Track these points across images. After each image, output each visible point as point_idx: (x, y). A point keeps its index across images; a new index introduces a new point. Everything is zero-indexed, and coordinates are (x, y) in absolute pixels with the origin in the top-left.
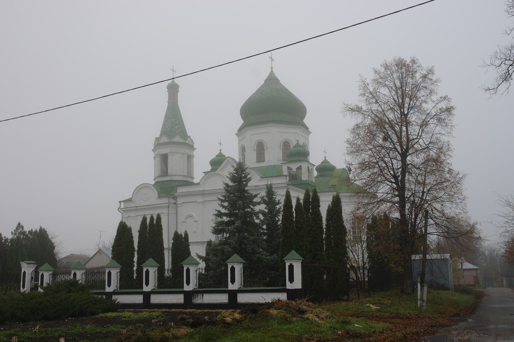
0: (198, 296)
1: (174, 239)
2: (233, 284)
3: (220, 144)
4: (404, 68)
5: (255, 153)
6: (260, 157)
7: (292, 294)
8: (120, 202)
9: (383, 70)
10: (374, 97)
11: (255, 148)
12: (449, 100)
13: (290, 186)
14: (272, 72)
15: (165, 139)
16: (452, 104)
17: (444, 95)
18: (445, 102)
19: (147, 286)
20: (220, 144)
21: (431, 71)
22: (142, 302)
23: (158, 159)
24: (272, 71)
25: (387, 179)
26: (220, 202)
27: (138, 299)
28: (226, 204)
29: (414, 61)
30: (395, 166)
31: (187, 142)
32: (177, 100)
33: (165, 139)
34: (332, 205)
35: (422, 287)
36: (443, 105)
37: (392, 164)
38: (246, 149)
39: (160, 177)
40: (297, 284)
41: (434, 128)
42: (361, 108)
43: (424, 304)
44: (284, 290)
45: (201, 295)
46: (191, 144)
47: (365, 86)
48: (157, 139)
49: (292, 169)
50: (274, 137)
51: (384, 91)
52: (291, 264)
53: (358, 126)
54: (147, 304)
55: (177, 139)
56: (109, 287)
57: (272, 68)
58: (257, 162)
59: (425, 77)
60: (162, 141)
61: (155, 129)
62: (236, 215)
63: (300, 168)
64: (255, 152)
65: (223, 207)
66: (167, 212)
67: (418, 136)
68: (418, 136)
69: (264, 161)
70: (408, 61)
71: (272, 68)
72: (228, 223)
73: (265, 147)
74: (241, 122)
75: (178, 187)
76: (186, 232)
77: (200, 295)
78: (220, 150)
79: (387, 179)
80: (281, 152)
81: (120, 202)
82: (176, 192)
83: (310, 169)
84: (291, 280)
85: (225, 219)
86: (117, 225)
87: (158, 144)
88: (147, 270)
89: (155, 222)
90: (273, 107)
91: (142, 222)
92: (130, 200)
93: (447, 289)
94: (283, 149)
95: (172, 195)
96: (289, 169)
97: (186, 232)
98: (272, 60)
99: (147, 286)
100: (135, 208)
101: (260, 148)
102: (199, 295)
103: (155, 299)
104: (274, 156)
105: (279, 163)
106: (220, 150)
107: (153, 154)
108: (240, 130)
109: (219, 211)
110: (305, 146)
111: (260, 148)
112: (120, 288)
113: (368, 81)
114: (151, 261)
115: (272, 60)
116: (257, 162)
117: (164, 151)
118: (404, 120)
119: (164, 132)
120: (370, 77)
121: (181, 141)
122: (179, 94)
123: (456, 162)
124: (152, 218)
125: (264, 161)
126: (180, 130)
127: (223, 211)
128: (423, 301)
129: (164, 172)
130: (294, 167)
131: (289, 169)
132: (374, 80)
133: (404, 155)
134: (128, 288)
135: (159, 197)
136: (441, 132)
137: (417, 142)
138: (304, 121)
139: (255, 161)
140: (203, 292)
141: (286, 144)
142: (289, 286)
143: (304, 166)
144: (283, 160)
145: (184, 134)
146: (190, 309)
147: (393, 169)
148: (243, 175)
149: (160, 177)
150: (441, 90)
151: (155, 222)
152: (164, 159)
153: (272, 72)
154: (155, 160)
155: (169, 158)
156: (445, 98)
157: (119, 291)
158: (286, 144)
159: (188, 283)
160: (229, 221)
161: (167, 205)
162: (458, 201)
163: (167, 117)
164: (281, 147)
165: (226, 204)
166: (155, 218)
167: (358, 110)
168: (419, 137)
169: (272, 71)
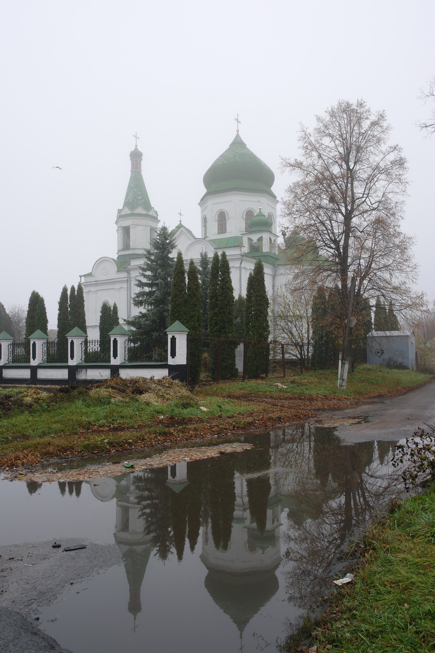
0: (82, 371)
1: (102, 312)
2: (115, 358)
3: (180, 214)
4: (350, 113)
5: (216, 224)
6: (222, 229)
7: (172, 369)
8: (81, 277)
9: (328, 118)
10: (311, 147)
11: (217, 219)
12: (400, 150)
13: (244, 257)
14: (238, 135)
15: (127, 211)
16: (403, 155)
17: (393, 144)
18: (396, 152)
19: (34, 360)
20: (180, 214)
21: (382, 117)
22: (29, 377)
23: (121, 231)
24: (238, 134)
25: (326, 245)
26: (141, 271)
27: (26, 374)
28: (149, 273)
29: (361, 105)
30: (336, 231)
31: (150, 213)
32: (140, 169)
33: (127, 211)
34: (254, 273)
35: (343, 364)
36: (392, 157)
37: (332, 226)
38: (208, 219)
39: (122, 250)
40: (181, 358)
41: (386, 186)
42: (302, 163)
43: (344, 384)
44: (166, 366)
45: (85, 370)
46: (154, 215)
47: (306, 137)
48: (120, 211)
49: (252, 240)
50: (237, 206)
51: (326, 141)
52: (173, 337)
53: (297, 185)
54: (34, 379)
55: (140, 210)
56: (72, 359)
57: (238, 131)
58: (218, 233)
59: (374, 124)
60: (123, 213)
61: (118, 199)
62: (157, 285)
63: (260, 239)
64: (217, 222)
65: (145, 276)
66: (126, 286)
67: (364, 194)
68: (364, 194)
69: (225, 232)
70: (354, 102)
71: (238, 131)
72: (150, 294)
73: (227, 218)
74: (204, 191)
75: (131, 260)
76: (115, 304)
77: (84, 370)
78: (180, 221)
79: (326, 245)
80: (244, 222)
81: (81, 277)
82: (129, 265)
83: (273, 240)
84: (173, 355)
85: (147, 289)
86: (29, 295)
87: (121, 216)
88: (34, 342)
89: (76, 293)
90: (237, 173)
91: (62, 293)
92: (90, 275)
93: (402, 367)
94: (246, 219)
95: (124, 268)
96: (250, 240)
97: (115, 304)
98: (238, 122)
99: (115, 358)
100: (95, 282)
101: (222, 219)
102: (83, 370)
103: (42, 374)
104: (236, 227)
105: (239, 235)
106: (180, 221)
107: (115, 227)
108: (202, 200)
109: (140, 281)
110: (271, 216)
111: (222, 219)
112: (86, 361)
113: (310, 130)
114: (38, 333)
115: (238, 122)
116: (218, 233)
117: (126, 223)
118: (350, 175)
119: (126, 204)
120: (312, 126)
121: (144, 212)
122: (142, 162)
123: (406, 225)
124: (73, 289)
125: (225, 232)
126: (143, 201)
127: (144, 280)
128: (343, 380)
129: (126, 245)
130: (255, 237)
131: (250, 240)
132: (316, 129)
133: (348, 217)
134: (59, 362)
135: (118, 271)
136: (394, 190)
137: (363, 202)
138: (271, 189)
139: (217, 232)
140: (87, 367)
141: (249, 214)
142: (171, 361)
143: (266, 236)
144: (246, 231)
145: (147, 205)
146: (40, 384)
147: (333, 233)
148: (168, 241)
149: (122, 250)
150: (391, 140)
151: (76, 293)
152: (126, 232)
153: (238, 135)
154: (118, 233)
155: (131, 230)
156: (395, 148)
157: (11, 364)
158: (249, 214)
159: (115, 356)
160: (150, 292)
161: (126, 279)
162: (408, 269)
163: (130, 188)
164: (244, 217)
165: (149, 273)
166: (76, 289)
167: (298, 165)
168: (365, 196)
169: (238, 134)
